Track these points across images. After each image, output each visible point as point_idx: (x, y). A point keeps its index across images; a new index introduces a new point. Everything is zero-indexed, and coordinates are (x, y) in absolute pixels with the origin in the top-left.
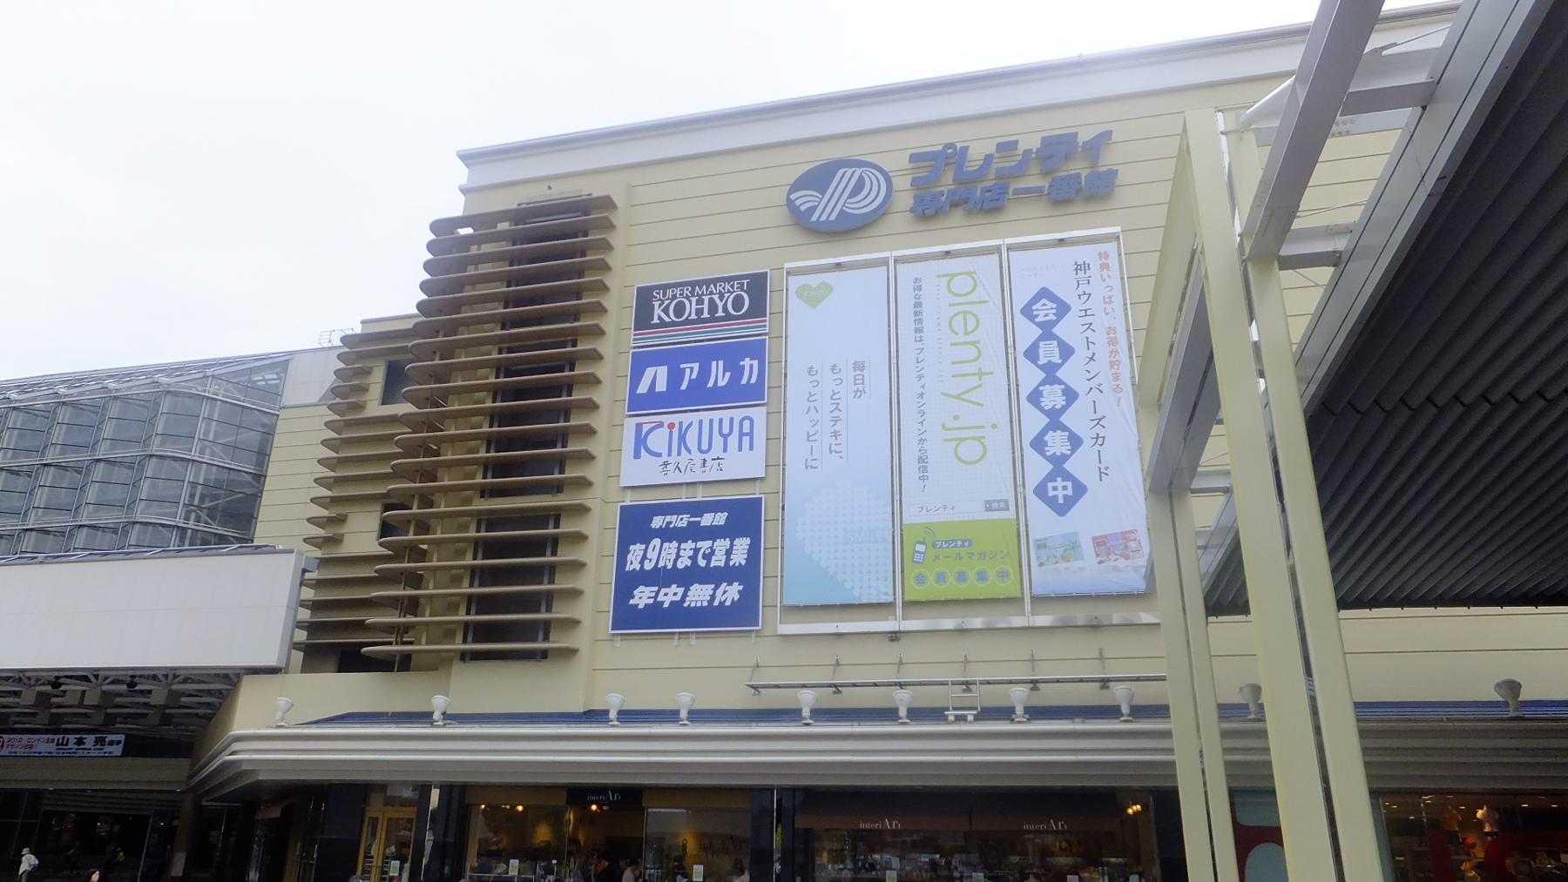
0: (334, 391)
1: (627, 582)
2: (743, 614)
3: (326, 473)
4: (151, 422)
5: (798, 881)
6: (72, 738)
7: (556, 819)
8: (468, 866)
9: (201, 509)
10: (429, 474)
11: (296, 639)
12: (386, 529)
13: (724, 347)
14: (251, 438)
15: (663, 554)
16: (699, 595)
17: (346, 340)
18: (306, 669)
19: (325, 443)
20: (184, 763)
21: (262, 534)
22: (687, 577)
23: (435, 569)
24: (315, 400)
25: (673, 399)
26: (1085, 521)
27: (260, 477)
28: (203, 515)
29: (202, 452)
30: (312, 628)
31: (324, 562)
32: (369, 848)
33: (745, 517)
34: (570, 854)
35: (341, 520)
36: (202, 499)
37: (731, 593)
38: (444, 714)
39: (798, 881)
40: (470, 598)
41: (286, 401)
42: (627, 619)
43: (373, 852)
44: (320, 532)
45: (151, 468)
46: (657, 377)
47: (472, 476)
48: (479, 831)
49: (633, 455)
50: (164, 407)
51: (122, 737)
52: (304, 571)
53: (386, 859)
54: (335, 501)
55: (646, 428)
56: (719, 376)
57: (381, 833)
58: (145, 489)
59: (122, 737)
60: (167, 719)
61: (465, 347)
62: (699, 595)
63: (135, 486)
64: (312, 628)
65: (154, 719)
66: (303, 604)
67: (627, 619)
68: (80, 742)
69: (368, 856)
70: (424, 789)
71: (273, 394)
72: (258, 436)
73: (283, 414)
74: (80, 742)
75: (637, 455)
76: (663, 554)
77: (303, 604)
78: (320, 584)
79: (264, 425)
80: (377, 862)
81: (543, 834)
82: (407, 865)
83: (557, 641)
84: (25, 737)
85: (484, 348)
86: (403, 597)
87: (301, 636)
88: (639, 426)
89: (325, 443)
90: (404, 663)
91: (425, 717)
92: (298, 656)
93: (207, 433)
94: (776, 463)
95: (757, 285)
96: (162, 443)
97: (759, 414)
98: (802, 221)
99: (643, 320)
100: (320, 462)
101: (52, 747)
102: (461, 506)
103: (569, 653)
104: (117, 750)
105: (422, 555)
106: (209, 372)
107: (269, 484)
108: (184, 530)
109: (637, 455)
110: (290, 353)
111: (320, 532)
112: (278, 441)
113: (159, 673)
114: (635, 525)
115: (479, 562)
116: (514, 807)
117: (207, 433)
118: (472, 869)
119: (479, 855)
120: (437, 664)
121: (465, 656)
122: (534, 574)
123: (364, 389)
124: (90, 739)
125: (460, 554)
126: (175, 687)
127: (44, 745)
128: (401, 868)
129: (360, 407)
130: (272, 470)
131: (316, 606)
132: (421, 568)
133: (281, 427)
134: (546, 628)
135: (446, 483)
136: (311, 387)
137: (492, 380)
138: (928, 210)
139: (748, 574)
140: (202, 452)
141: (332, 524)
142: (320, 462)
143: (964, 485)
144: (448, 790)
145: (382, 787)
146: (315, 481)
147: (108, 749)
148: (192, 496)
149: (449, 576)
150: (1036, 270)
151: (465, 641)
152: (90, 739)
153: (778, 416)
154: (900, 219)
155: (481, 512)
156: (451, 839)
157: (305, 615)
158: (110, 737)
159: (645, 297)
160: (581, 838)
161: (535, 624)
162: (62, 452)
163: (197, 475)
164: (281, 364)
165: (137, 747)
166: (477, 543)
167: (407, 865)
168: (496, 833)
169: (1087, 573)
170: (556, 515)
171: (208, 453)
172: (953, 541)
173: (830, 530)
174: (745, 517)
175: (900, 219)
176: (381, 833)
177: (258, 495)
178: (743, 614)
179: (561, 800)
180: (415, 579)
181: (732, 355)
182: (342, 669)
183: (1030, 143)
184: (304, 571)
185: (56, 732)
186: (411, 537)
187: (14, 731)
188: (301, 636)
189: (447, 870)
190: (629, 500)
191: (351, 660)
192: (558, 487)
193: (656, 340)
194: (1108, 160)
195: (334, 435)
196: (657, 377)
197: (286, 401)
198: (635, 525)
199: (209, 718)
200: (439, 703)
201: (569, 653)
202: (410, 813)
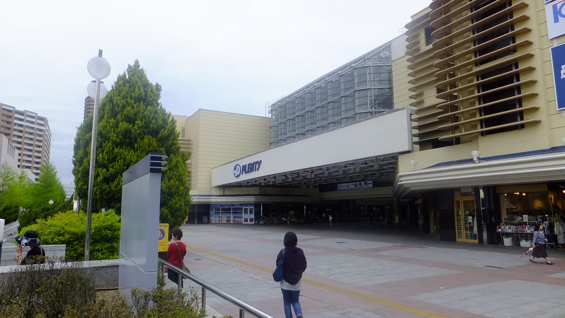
0: (407, 54)
3: (412, 86)
4: (353, 80)
6: (358, 183)
7: (544, 197)
8: (503, 218)
9: (375, 104)
10: (456, 118)
11: (414, 141)
12: (439, 91)
14: (384, 76)
17: (406, 26)
18: (421, 149)
19: (409, 75)
20: (391, 188)
21: (396, 106)
23: (463, 113)
24: (403, 55)
27: (391, 89)
28: (376, 106)
29: (371, 85)
30: (419, 135)
31: (418, 112)
32: (458, 212)
34: (556, 212)
35: (421, 94)
36: (375, 101)
38: (478, 158)
40: (481, 121)
41: (393, 59)
43: (460, 213)
44: (415, 101)
45: (357, 95)
47: (472, 81)
48: (505, 205)
50: (356, 74)
51: (371, 182)
52: (411, 115)
53: (466, 216)
54: (418, 88)
55: (559, 6)
57: (462, 205)
58: (357, 102)
59: (371, 182)
60: (382, 174)
61: (455, 16)
63: (354, 102)
64: (419, 135)
65: (378, 175)
66: (414, 128)
68: (360, 184)
69: (458, 215)
70: (476, 189)
71: (388, 58)
72: (387, 75)
73: (393, 64)
74: (360, 184)
75: (556, 20)
77: (414, 128)
78: (419, 119)
79: (388, 70)
80: (462, 217)
81: (538, 204)
82: (475, 218)
83: (528, 119)
84: (346, 184)
85: (465, 34)
86: (451, 126)
87: (416, 139)
88: (555, 7)
89: (409, 75)
90: (457, 141)
91: (471, 161)
92: (418, 146)
93: (370, 79)
96: (358, 86)
100: (409, 82)
101: (353, 186)
102: (468, 71)
103: (536, 123)
104: (371, 186)
105: (456, 108)
106: (366, 58)
107: (395, 90)
108: (372, 112)
109: (556, 20)
110: (390, 41)
111: (415, 101)
112: (394, 74)
113: (374, 159)
115: (482, 105)
116: (521, 194)
117: (370, 79)
118: (505, 219)
119: (507, 214)
120: (472, 139)
121: (483, 134)
122: (509, 79)
123: (418, 42)
124: (363, 183)
125: (473, 104)
126: (380, 163)
127: (351, 186)
128: (473, 219)
129: (418, 50)
130: (395, 84)
131: (419, 128)
132: (456, 103)
133: (394, 69)
134: (521, 114)
135: (460, 76)
136: (400, 51)
137: (472, 36)
140: (371, 85)
141: (418, 97)
142: (409, 82)
144: (487, 189)
145: (458, 189)
146: (409, 90)
147: (368, 185)
148: (371, 101)
149: (469, 104)
151: (482, 128)
152: (363, 183)
155: (477, 73)
156: (492, 208)
157: (416, 132)
158: (368, 182)
160: (560, 205)
161: (515, 114)
162: (332, 98)
163: (371, 94)
164: (388, 47)
165: (376, 184)
166: (479, 98)
167: (475, 218)
168: (514, 205)
170: (516, 63)
171: (373, 85)
176: (462, 205)
177: (392, 95)
179: (546, 189)
180: (456, 118)
182: (435, 147)
184: (411, 115)
185: (353, 182)
186: (449, 91)
187: (343, 183)
188: (416, 139)
189: (493, 219)
190: (556, 44)
191: (437, 144)
192: (514, 50)
195: (412, 71)
197: (393, 59)
199: (394, 172)
200: (475, 154)
201: (536, 123)
202: (473, 198)
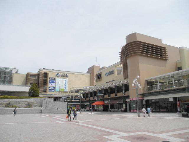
1: (49, 90)
2: (54, 91)
5: (1, 94)
13: (53, 81)
15: (50, 89)
16: (52, 90)
22: (52, 90)
25: (51, 82)
26: (66, 89)
33: (54, 88)
37: (53, 90)
39: (1, 94)
42: (49, 91)
46: (50, 81)
49: (50, 85)
56: (53, 82)
62: (52, 90)
67: (49, 91)
76: (50, 89)
94: (55, 85)
95: (55, 78)
97: (55, 84)
98: (57, 76)
99: (50, 79)
114: (50, 87)
138: (61, 76)
139: (54, 90)
143: (62, 87)
146: (40, 73)
150: (65, 80)
153: (55, 84)
154: (60, 77)
159: (50, 78)
169: (66, 91)
172: (62, 89)
173: (57, 89)
174: (54, 88)
175: (60, 77)
178: (54, 91)
181: (54, 81)
183: (66, 74)
193: (50, 80)
194: (68, 76)
196: (50, 81)
198: (50, 87)
199: (100, 76)
